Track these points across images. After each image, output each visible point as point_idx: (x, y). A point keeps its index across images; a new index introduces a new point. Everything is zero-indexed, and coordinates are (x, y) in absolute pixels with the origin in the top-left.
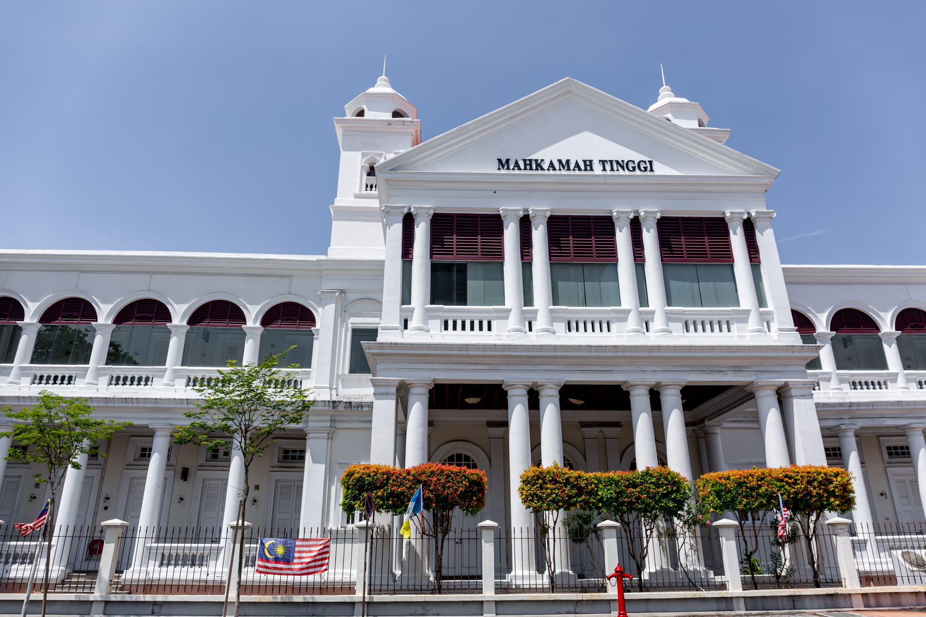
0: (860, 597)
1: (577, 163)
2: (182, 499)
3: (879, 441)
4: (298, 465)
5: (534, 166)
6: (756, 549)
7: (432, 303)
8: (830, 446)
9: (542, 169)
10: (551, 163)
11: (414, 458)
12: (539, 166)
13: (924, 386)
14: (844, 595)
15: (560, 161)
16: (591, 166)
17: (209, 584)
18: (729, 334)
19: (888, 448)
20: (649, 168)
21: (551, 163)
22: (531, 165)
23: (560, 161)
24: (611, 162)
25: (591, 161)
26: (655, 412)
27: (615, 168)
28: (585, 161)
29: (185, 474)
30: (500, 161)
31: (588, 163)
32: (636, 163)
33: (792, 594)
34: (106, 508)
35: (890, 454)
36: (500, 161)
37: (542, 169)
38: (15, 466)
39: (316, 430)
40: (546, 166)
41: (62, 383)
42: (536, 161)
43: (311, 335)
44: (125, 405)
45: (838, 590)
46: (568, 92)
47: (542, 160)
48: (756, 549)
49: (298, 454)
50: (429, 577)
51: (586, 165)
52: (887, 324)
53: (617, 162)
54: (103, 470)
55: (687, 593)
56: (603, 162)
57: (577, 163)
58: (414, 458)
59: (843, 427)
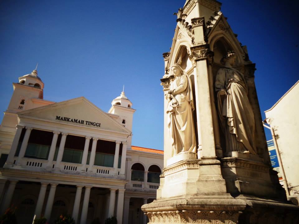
1: (79, 121)
6: (173, 66)
8: (146, 202)
9: (69, 121)
10: (72, 120)
11: (273, 165)
12: (68, 120)
15: (75, 120)
16: (83, 122)
18: (71, 171)
23: (75, 120)
24: (89, 122)
28: (82, 121)
30: (57, 117)
36: (57, 117)
37: (69, 121)
40: (70, 120)
46: (83, 100)
47: (70, 119)
48: (173, 66)
50: (232, 130)
51: (82, 122)
53: (91, 122)
56: (87, 122)
57: (79, 121)
58: (273, 165)
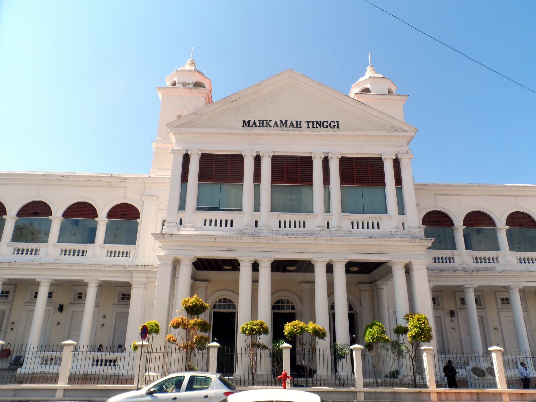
0: (436, 394)
2: (59, 324)
3: (495, 294)
4: (81, 302)
5: (265, 125)
6: (379, 362)
7: (342, 212)
9: (270, 126)
10: (276, 122)
12: (268, 125)
13: (535, 261)
14: (426, 393)
15: (281, 121)
16: (300, 124)
17: (513, 379)
19: (502, 299)
20: (336, 127)
21: (276, 122)
22: (263, 123)
23: (281, 121)
24: (313, 122)
25: (300, 122)
26: (329, 274)
27: (315, 126)
28: (297, 121)
29: (61, 308)
30: (244, 121)
31: (299, 123)
32: (329, 123)
33: (393, 391)
34: (12, 329)
35: (503, 303)
36: (244, 121)
37: (270, 126)
38: (73, 305)
39: (138, 283)
41: (22, 254)
42: (267, 121)
43: (50, 221)
44: (70, 268)
45: (352, 389)
47: (270, 121)
49: (4, 294)
51: (297, 124)
52: (501, 222)
53: (317, 122)
54: (11, 307)
55: (406, 389)
56: (308, 122)
59: (466, 286)
